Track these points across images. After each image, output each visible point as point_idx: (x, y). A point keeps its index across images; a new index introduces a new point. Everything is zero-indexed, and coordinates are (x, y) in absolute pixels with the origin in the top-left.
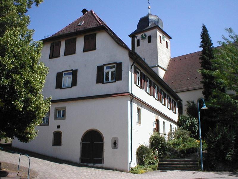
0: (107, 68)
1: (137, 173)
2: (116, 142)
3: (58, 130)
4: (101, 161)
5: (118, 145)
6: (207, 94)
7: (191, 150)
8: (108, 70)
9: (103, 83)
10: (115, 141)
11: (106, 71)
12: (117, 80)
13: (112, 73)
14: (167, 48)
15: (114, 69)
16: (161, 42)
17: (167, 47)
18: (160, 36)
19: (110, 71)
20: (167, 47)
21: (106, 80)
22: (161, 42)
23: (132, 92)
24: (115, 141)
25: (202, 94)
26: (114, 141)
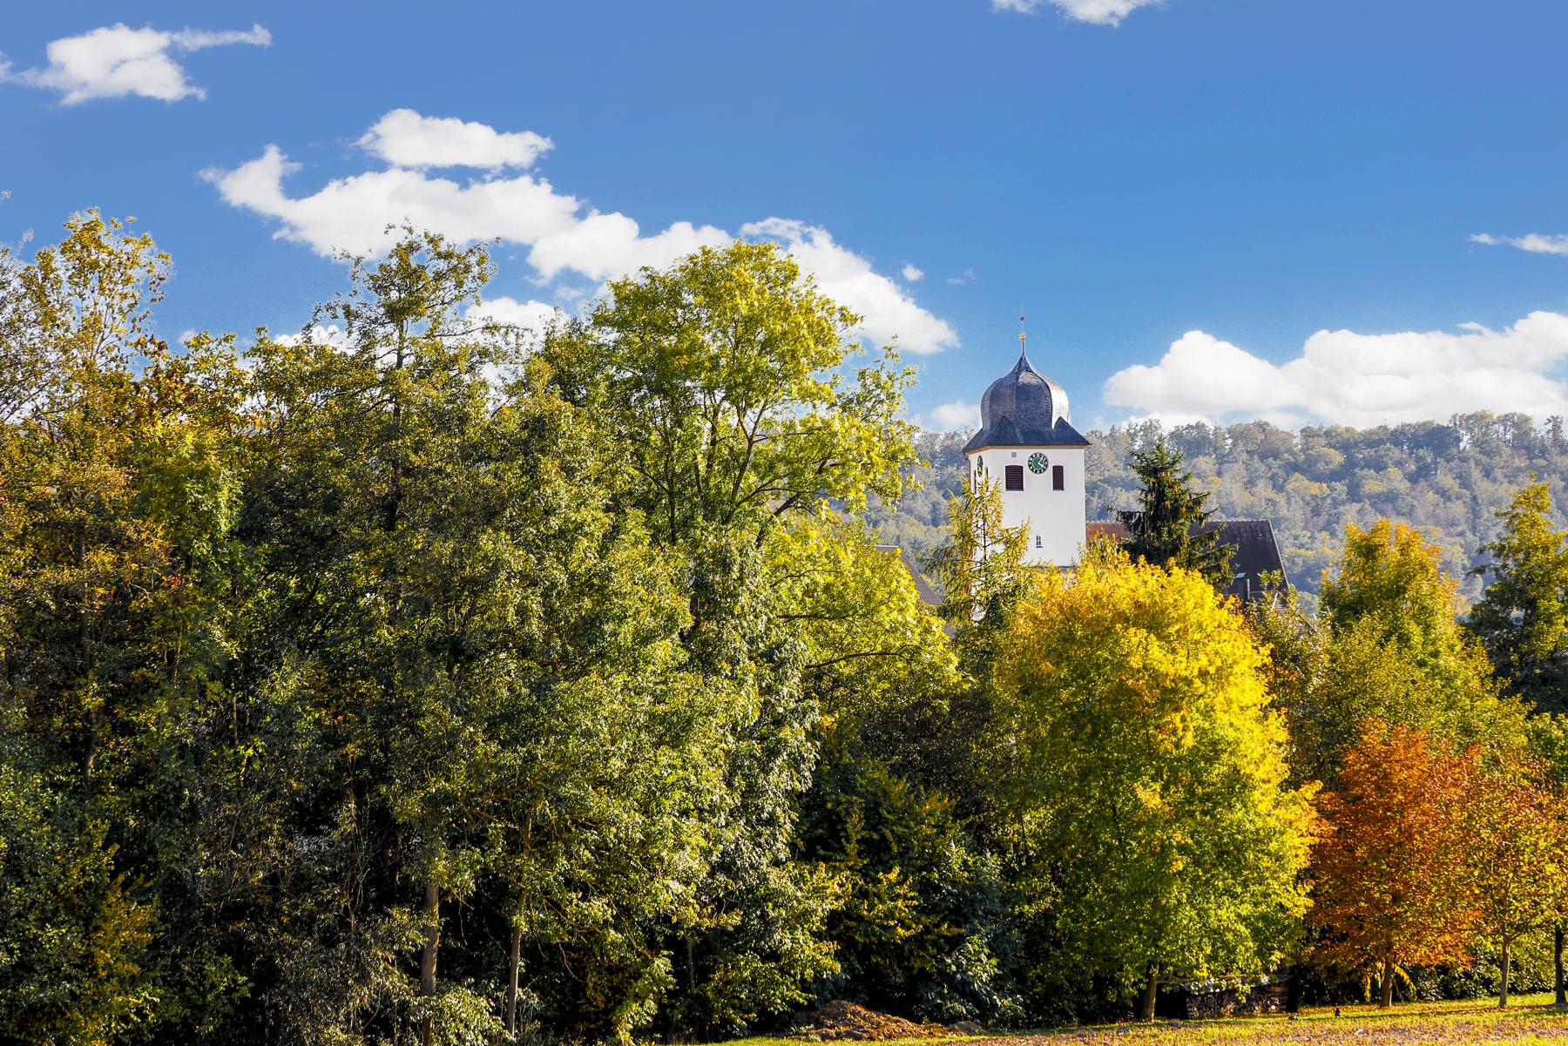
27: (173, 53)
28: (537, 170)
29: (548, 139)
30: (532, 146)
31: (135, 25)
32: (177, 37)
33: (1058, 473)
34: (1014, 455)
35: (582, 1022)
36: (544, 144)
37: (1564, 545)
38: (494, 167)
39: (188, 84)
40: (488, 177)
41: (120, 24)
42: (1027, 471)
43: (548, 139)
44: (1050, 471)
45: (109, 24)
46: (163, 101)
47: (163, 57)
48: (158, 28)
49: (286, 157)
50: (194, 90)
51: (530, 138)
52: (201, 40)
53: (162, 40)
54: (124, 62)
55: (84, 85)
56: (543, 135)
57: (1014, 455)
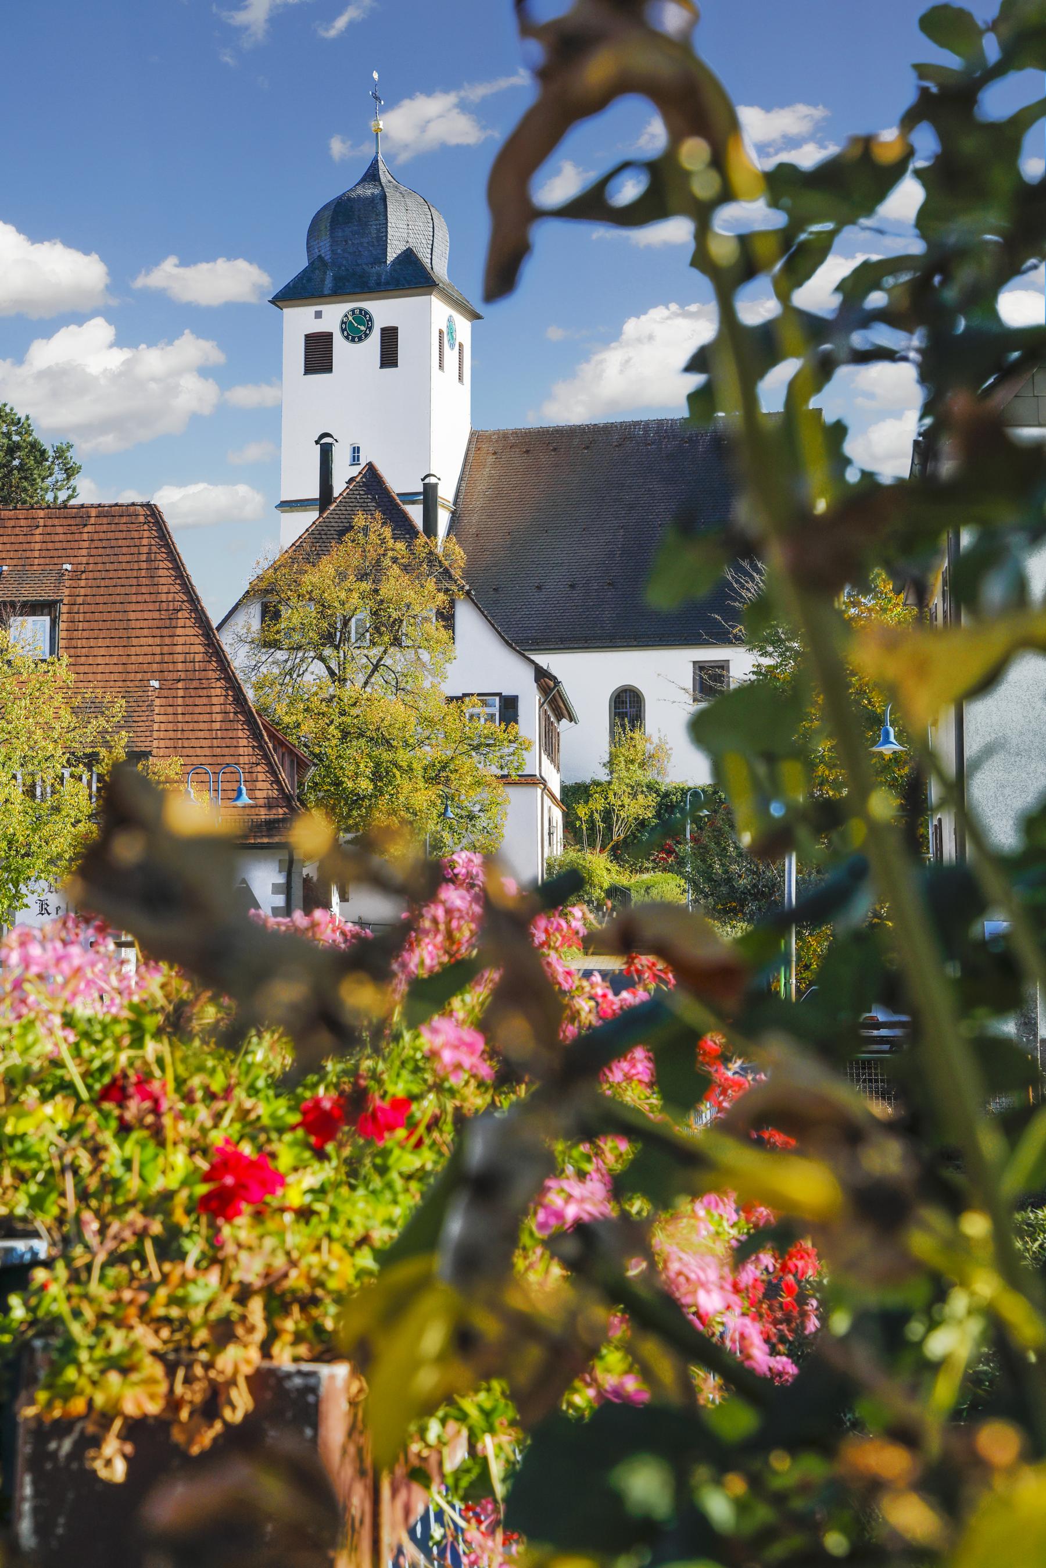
17: (461, 378)
20: (461, 378)
22: (441, 366)
27: (463, 106)
28: (819, 135)
29: (821, 107)
30: (806, 116)
31: (429, 91)
32: (462, 94)
33: (390, 336)
34: (318, 315)
35: (762, 1080)
36: (818, 113)
37: (8, 1179)
38: (774, 141)
39: (483, 128)
40: (771, 150)
41: (418, 94)
42: (339, 343)
43: (821, 107)
44: (375, 337)
45: (410, 96)
46: (468, 146)
47: (456, 111)
48: (446, 91)
49: (581, 169)
50: (489, 132)
51: (802, 109)
52: (479, 92)
53: (451, 99)
54: (428, 122)
55: (406, 146)
56: (815, 105)
57: (318, 315)
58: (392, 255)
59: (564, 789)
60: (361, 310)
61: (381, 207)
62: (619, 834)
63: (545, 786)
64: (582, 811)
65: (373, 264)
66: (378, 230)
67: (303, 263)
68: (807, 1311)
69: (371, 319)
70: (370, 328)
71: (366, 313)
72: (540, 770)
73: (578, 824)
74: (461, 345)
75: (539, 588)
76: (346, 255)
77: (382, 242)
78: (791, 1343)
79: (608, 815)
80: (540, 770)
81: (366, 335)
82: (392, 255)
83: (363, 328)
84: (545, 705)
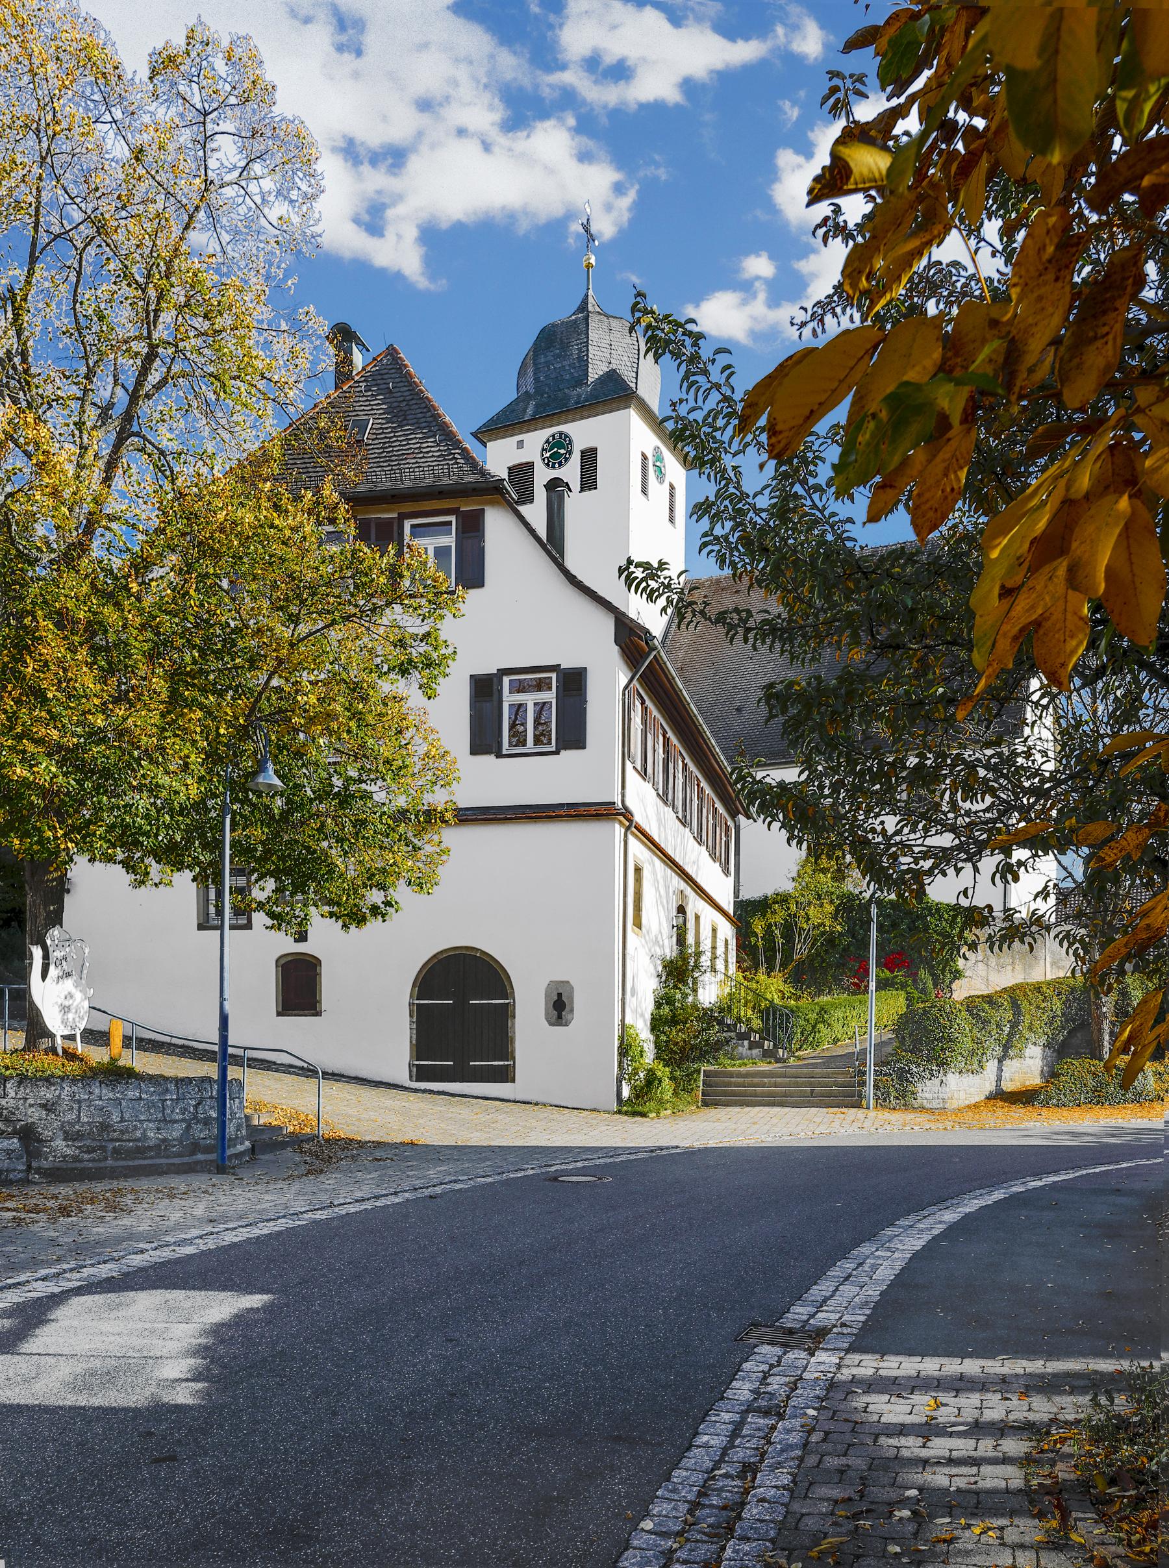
0: (519, 688)
1: (1098, 50)
2: (564, 999)
3: (301, 948)
4: (505, 1075)
5: (572, 1010)
6: (277, 210)
7: (759, 213)
8: (519, 698)
9: (499, 755)
10: (560, 995)
11: (509, 699)
12: (565, 749)
13: (541, 707)
14: (669, 524)
15: (550, 696)
16: (644, 491)
17: (672, 519)
18: (643, 455)
19: (530, 699)
20: (672, 519)
21: (537, 741)
22: (644, 491)
23: (628, 803)
24: (560, 995)
25: (386, 233)
26: (556, 998)
33: (589, 457)
34: (520, 444)
44: (576, 458)
57: (520, 444)
58: (593, 376)
59: (740, 905)
60: (561, 434)
61: (582, 327)
62: (801, 950)
63: (630, 821)
64: (758, 927)
65: (574, 387)
66: (579, 350)
67: (514, 396)
68: (774, 31)
69: (571, 443)
70: (570, 452)
71: (566, 436)
72: (623, 796)
73: (753, 940)
74: (672, 487)
75: (739, 710)
76: (548, 382)
77: (583, 363)
78: (959, 848)
79: (789, 930)
80: (623, 796)
81: (566, 460)
82: (593, 376)
83: (562, 451)
84: (635, 682)
